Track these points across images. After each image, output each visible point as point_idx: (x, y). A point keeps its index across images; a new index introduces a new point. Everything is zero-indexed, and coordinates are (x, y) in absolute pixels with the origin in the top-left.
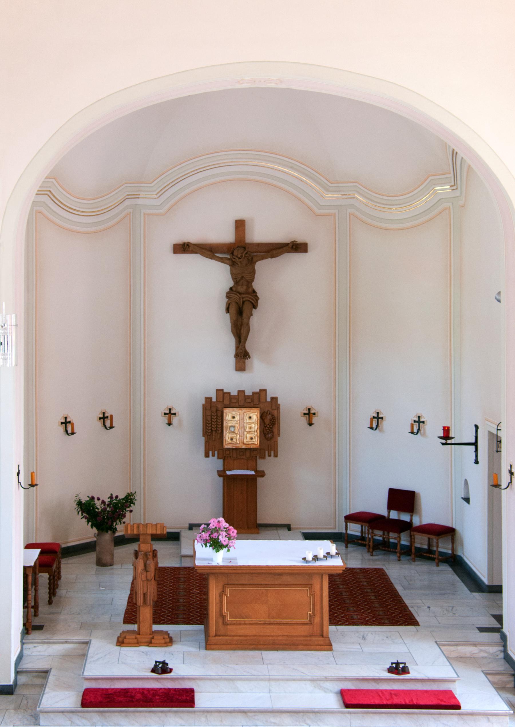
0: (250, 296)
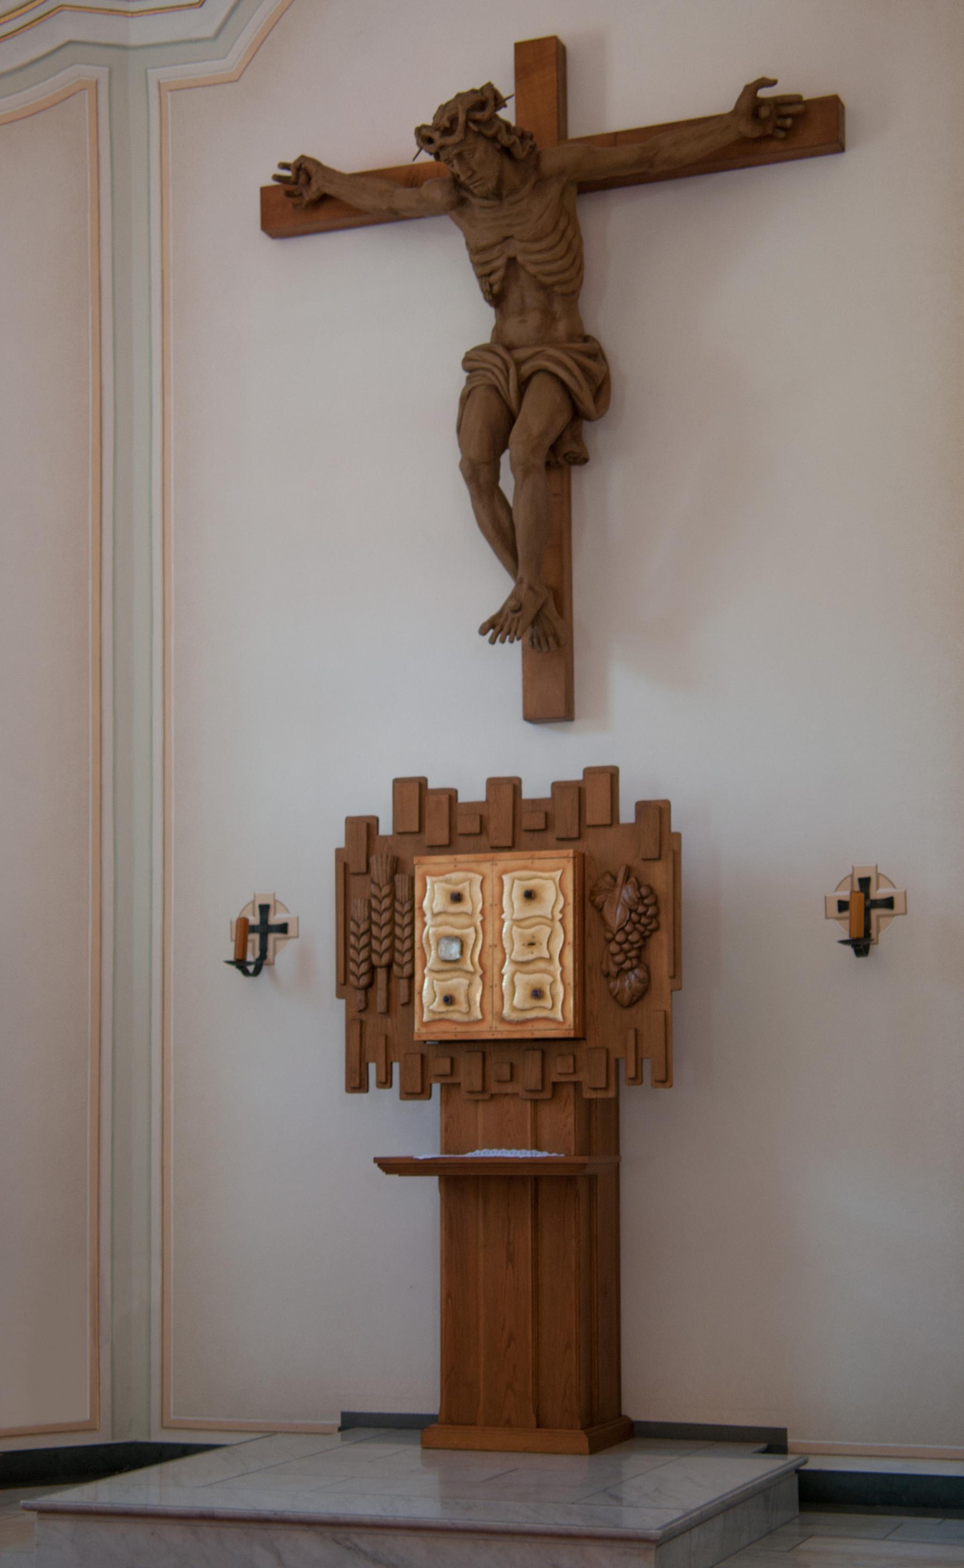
0: (551, 351)
